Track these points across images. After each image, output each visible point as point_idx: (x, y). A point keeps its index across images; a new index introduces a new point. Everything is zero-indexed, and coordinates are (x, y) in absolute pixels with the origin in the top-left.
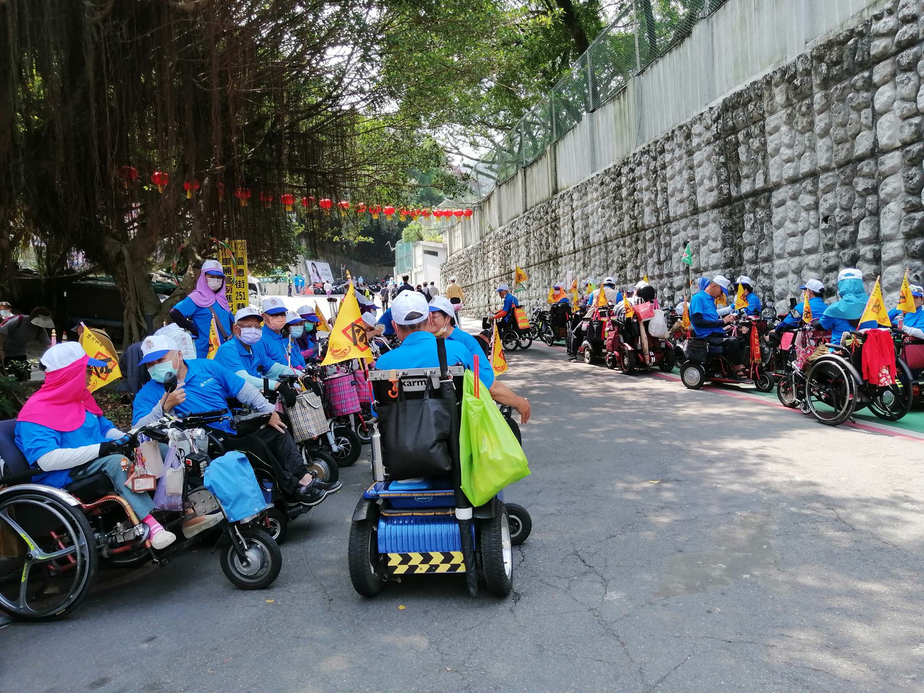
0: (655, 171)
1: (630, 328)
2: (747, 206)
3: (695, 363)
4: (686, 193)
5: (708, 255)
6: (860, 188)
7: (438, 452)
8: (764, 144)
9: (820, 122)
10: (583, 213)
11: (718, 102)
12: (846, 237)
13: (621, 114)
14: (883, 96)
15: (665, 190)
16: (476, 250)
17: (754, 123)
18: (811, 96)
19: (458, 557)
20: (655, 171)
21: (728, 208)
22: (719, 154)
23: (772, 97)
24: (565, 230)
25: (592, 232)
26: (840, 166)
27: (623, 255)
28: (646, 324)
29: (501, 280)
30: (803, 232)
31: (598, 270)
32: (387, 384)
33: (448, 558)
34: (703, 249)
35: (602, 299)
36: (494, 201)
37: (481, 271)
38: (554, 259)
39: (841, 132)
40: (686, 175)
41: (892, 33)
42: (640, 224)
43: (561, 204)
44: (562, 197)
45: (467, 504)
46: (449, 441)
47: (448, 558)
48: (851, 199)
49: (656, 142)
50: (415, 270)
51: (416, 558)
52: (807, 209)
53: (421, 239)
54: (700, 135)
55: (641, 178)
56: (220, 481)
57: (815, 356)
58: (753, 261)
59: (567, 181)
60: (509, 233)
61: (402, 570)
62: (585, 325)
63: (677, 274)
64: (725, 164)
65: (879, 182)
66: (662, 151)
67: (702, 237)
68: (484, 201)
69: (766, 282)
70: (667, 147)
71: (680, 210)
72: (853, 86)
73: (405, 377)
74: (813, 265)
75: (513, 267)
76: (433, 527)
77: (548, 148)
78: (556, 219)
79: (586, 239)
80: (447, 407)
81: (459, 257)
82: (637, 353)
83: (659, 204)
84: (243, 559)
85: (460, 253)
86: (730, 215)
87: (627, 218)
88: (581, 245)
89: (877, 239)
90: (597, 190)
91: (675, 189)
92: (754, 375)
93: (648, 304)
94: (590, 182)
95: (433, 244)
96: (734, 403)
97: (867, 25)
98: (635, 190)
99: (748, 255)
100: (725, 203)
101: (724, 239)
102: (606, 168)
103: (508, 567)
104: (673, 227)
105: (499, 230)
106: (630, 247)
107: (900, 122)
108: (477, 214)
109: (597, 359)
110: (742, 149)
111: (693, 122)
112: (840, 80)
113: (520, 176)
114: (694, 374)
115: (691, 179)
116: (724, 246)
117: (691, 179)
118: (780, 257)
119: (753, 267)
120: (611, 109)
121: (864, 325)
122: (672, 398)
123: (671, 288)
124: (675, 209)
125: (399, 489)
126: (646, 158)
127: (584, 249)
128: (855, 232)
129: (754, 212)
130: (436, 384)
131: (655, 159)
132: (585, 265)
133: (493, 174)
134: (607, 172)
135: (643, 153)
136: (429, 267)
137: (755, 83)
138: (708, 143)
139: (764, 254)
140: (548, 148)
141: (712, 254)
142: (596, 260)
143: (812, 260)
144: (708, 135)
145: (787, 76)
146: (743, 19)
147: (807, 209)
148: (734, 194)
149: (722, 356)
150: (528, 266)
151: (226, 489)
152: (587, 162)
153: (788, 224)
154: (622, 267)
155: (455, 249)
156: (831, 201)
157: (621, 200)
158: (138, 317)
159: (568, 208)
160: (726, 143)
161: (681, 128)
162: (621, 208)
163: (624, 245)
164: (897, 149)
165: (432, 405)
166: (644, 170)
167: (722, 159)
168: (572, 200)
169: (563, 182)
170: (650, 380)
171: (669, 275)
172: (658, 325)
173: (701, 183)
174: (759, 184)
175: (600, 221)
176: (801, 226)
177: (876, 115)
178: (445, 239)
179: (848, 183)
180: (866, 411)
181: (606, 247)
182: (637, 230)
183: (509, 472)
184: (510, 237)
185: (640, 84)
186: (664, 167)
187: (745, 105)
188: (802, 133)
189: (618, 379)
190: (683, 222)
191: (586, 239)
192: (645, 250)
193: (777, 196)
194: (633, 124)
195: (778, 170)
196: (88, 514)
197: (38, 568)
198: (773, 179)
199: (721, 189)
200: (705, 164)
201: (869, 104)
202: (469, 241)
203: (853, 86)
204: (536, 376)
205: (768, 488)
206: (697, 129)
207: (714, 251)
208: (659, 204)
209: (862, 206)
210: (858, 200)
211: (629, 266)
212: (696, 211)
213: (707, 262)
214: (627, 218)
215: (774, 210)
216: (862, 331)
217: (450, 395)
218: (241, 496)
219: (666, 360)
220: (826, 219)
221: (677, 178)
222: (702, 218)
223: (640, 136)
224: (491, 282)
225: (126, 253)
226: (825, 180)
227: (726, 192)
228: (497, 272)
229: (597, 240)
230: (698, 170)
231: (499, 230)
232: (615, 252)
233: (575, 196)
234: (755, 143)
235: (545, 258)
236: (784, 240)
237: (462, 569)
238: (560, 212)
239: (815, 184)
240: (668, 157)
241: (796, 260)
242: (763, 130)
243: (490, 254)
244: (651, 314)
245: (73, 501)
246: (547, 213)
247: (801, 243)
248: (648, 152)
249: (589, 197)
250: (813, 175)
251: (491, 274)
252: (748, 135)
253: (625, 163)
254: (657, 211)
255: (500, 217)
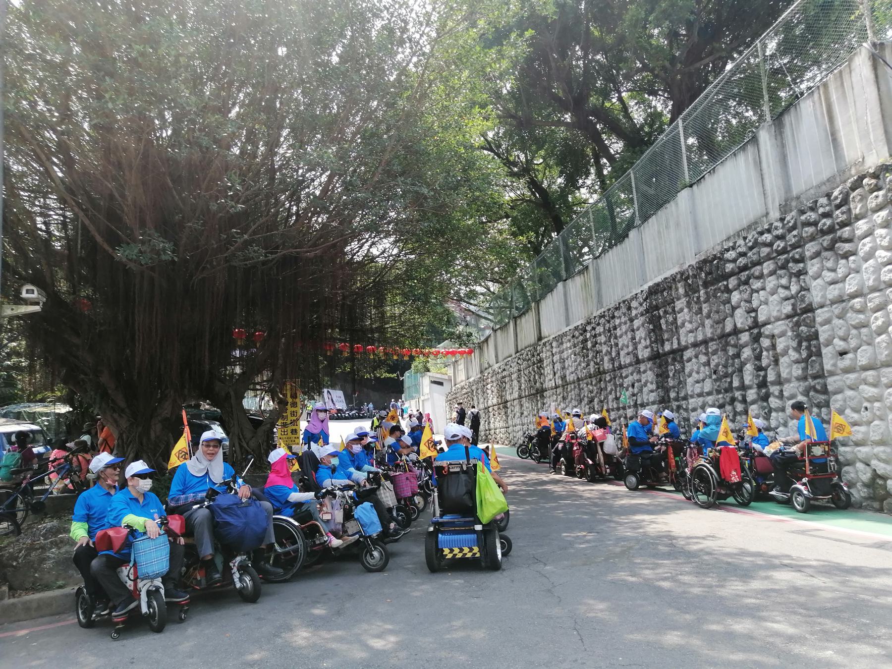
0: (609, 331)
1: (591, 447)
2: (670, 360)
3: (633, 473)
4: (631, 348)
5: (648, 394)
6: (731, 353)
7: (466, 497)
8: (675, 319)
9: (705, 308)
10: (560, 358)
11: (645, 287)
12: (727, 385)
13: (586, 285)
14: (735, 297)
15: (617, 345)
16: (477, 382)
17: (669, 304)
18: (699, 291)
19: (476, 549)
20: (609, 331)
21: (658, 361)
22: (649, 323)
23: (677, 289)
24: (548, 370)
25: (568, 373)
26: (719, 338)
27: (591, 392)
28: (602, 444)
29: (499, 408)
30: (703, 380)
31: (574, 403)
32: (442, 468)
33: (471, 550)
34: (645, 389)
35: (571, 427)
36: (491, 342)
37: (482, 400)
38: (541, 392)
39: (716, 317)
40: (629, 335)
41: (734, 261)
42: (601, 369)
43: (544, 349)
44: (544, 344)
45: (480, 523)
46: (471, 493)
47: (471, 550)
48: (727, 360)
49: (609, 310)
50: (422, 398)
51: (456, 550)
52: (705, 365)
53: (429, 371)
54: (636, 308)
55: (600, 335)
56: (362, 516)
57: (695, 465)
58: (677, 399)
59: (550, 329)
60: (504, 370)
61: (450, 556)
62: (560, 446)
63: (629, 407)
64: (653, 330)
65: (740, 350)
66: (613, 317)
67: (643, 381)
68: (483, 342)
69: (685, 414)
70: (616, 314)
71: (628, 361)
72: (719, 289)
73: (451, 464)
74: (871, 381)
75: (508, 398)
76: (464, 536)
77: (533, 304)
78: (541, 361)
79: (563, 378)
80: (470, 478)
81: (462, 388)
82: (596, 465)
83: (614, 354)
84: (372, 555)
85: (462, 384)
86: (660, 366)
87: (592, 363)
88: (560, 382)
89: (743, 387)
90: (570, 341)
91: (623, 345)
92: (672, 480)
93: (602, 430)
94: (565, 334)
95: (439, 376)
96: (654, 497)
97: (722, 253)
98: (596, 343)
99: (673, 395)
100: (655, 357)
101: (657, 383)
102: (576, 325)
103: (500, 556)
104: (624, 372)
105: (496, 367)
106: (595, 385)
107: (746, 315)
108: (477, 352)
109: (570, 472)
110: (663, 321)
111: (632, 299)
112: (713, 284)
113: (511, 324)
114: (633, 479)
115: (633, 338)
116: (658, 388)
117: (633, 338)
118: (692, 397)
119: (677, 403)
120: (578, 280)
121: (719, 444)
122: (616, 496)
123: (626, 418)
124: (625, 360)
125: (446, 518)
126: (602, 321)
127: (563, 386)
128: (731, 382)
129: (674, 365)
130: (465, 468)
131: (609, 322)
132: (564, 398)
133: (490, 317)
134: (576, 328)
135: (601, 317)
136: (436, 395)
137: (666, 278)
138: (642, 315)
139: (682, 395)
140: (533, 304)
141: (650, 394)
142: (572, 395)
143: (710, 399)
144: (641, 309)
145: (683, 276)
146: (659, 232)
147: (705, 365)
148: (661, 351)
149: (650, 466)
150: (520, 397)
151: (365, 520)
152: (563, 318)
153: (694, 374)
154: (591, 401)
155: (458, 380)
156: (716, 361)
157: (587, 350)
158: (240, 439)
159: (549, 354)
160: (653, 316)
161: (624, 302)
162: (588, 356)
163: (591, 384)
164: (747, 330)
165: (463, 477)
166: (602, 330)
167: (651, 327)
168: (552, 347)
169: (545, 331)
170: (606, 485)
171: (624, 408)
172: (611, 444)
173: (640, 342)
174: (675, 346)
175: (574, 368)
176: (701, 376)
177: (734, 309)
178: (450, 371)
179: (725, 350)
180: (731, 500)
181: (579, 385)
182: (600, 373)
183: (499, 507)
184: (505, 373)
185: (597, 264)
186: (615, 328)
187: (662, 292)
188: (697, 314)
189: (582, 484)
190: (631, 369)
191: (563, 378)
192: (606, 388)
193: (688, 354)
194: (594, 293)
195: (686, 338)
196: (302, 529)
197: (278, 556)
198: (683, 343)
199: (652, 347)
200: (641, 329)
201: (729, 301)
202: (470, 374)
203: (719, 289)
204: (524, 483)
205: (645, 534)
206: (634, 304)
207: (652, 391)
208: (614, 354)
209: (733, 365)
210: (730, 361)
211: (596, 400)
212: (638, 362)
213: (692, 391)
214: (592, 363)
215: (686, 364)
216: (719, 448)
217: (471, 473)
218: (372, 523)
219: (613, 470)
220: (715, 372)
221: (624, 337)
222: (642, 367)
223: (600, 302)
224: (491, 409)
225: (232, 393)
226: (712, 346)
227: (655, 349)
228: (495, 401)
229: (572, 379)
230: (637, 333)
231: (496, 367)
232: (586, 389)
233: (554, 344)
234: (670, 318)
235: (533, 392)
236: (693, 385)
237: (478, 555)
238: (543, 355)
239: (707, 349)
240: (617, 322)
241: (701, 399)
242: (674, 310)
243: (489, 386)
244: (604, 437)
245: (296, 524)
246: (533, 356)
247: (702, 388)
248: (604, 316)
249: (565, 346)
250: (705, 342)
251: (490, 403)
252: (666, 312)
253: (589, 323)
254: (612, 360)
255: (497, 356)
